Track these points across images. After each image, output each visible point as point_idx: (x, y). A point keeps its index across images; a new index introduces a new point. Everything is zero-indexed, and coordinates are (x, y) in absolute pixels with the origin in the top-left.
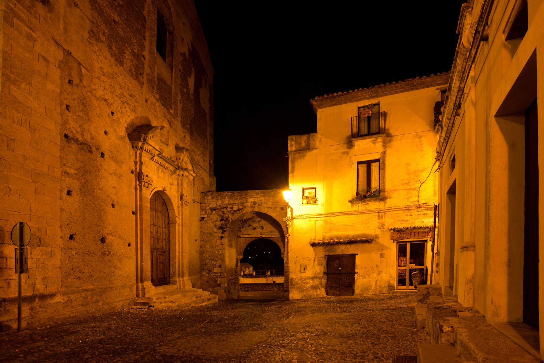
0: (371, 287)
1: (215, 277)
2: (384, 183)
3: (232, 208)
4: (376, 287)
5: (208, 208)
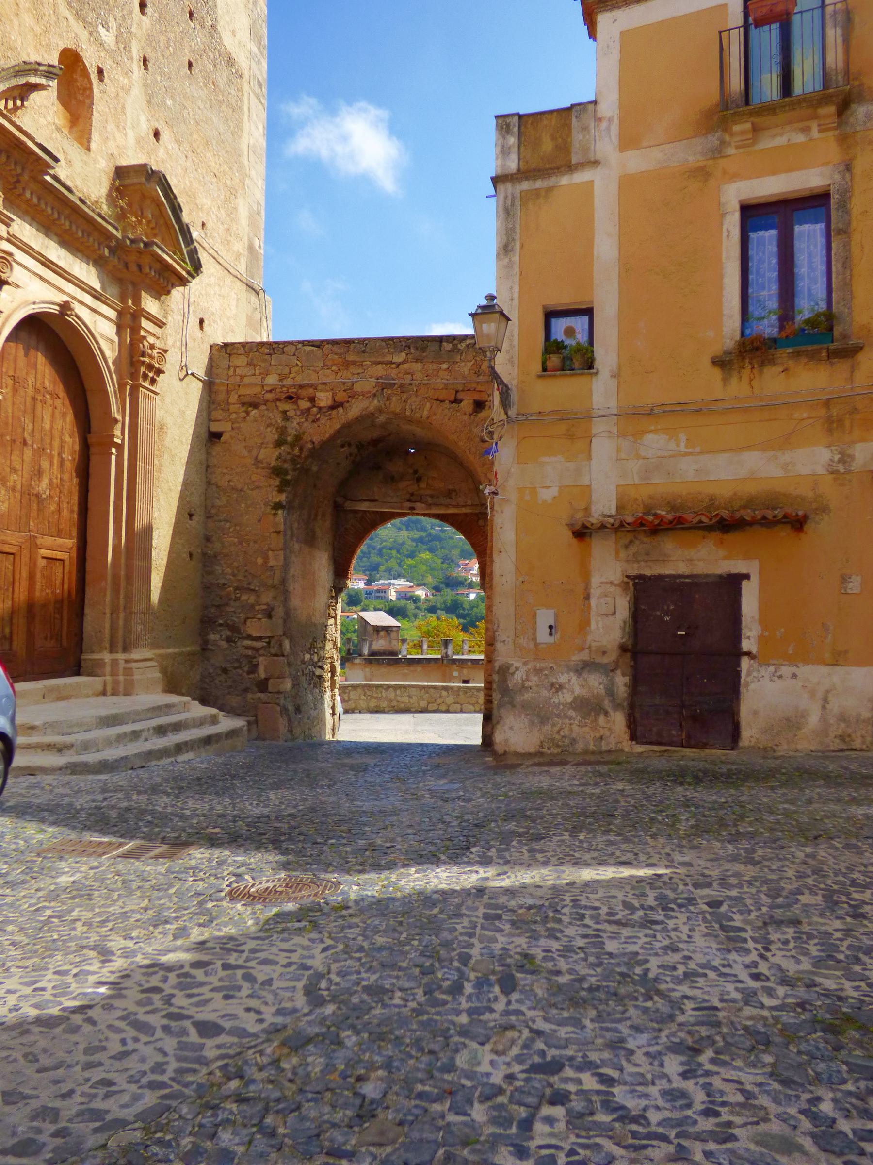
0: (803, 716)
1: (250, 653)
2: (847, 285)
3: (312, 400)
4: (823, 719)
5: (234, 398)
